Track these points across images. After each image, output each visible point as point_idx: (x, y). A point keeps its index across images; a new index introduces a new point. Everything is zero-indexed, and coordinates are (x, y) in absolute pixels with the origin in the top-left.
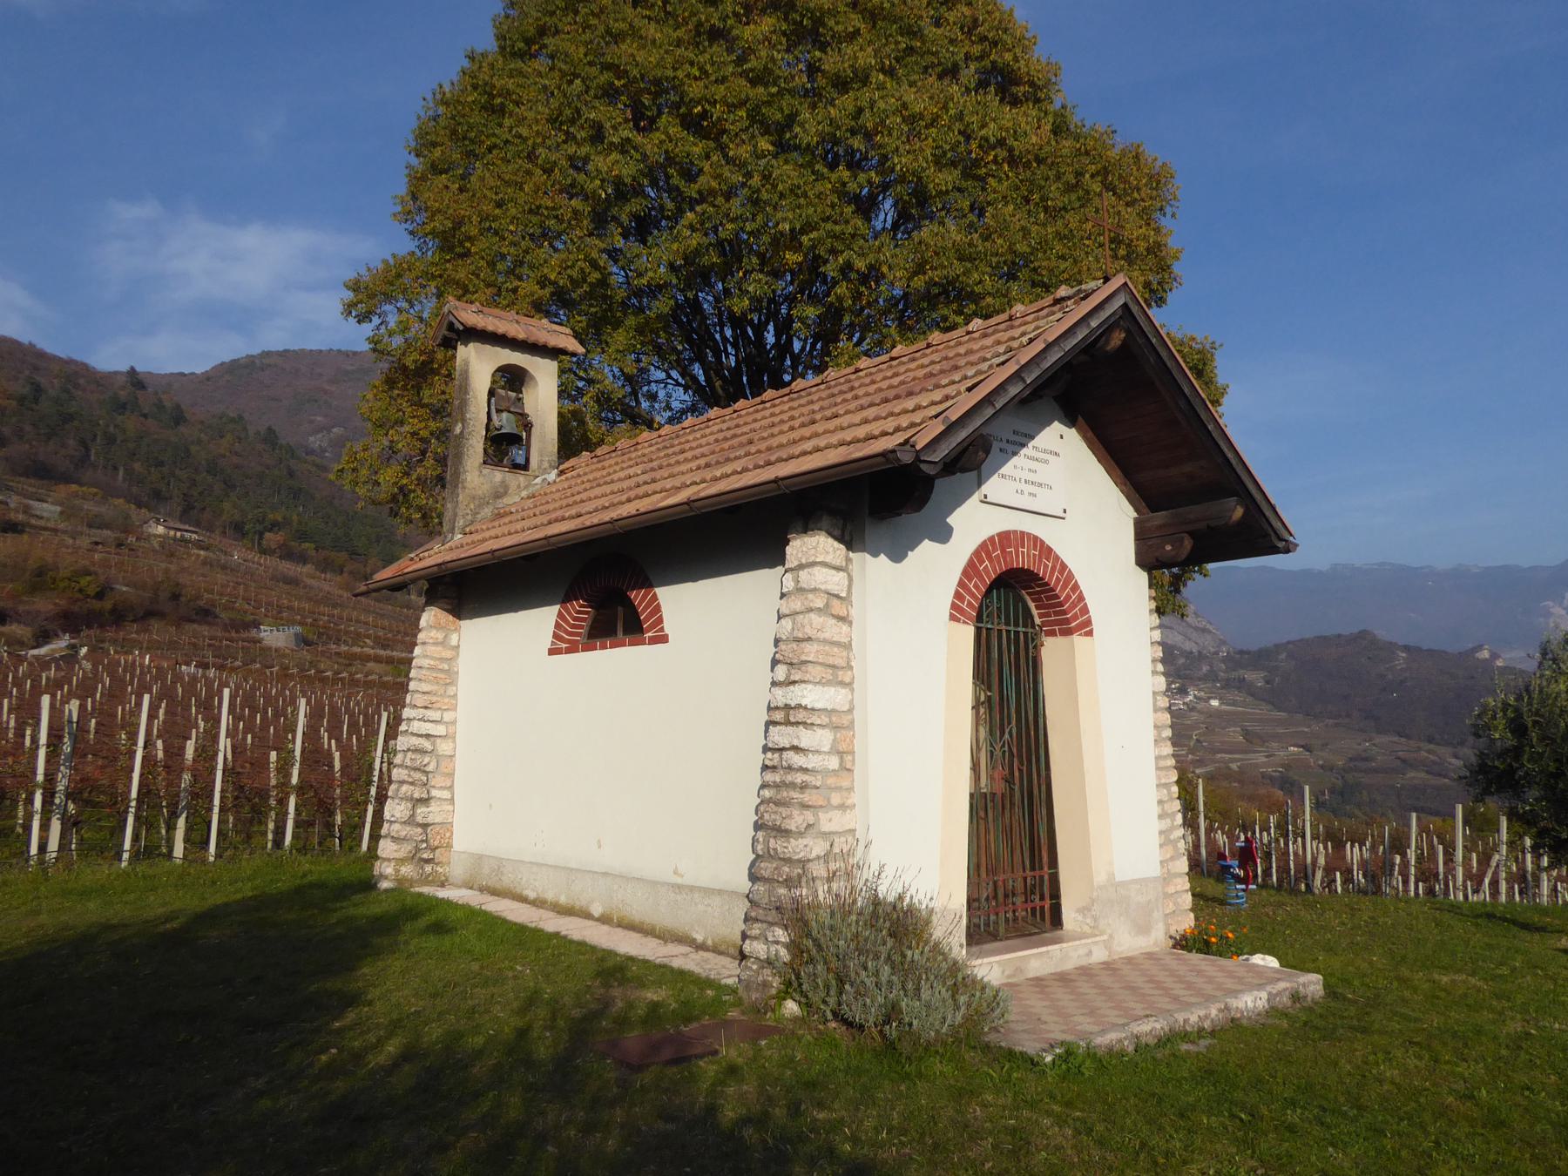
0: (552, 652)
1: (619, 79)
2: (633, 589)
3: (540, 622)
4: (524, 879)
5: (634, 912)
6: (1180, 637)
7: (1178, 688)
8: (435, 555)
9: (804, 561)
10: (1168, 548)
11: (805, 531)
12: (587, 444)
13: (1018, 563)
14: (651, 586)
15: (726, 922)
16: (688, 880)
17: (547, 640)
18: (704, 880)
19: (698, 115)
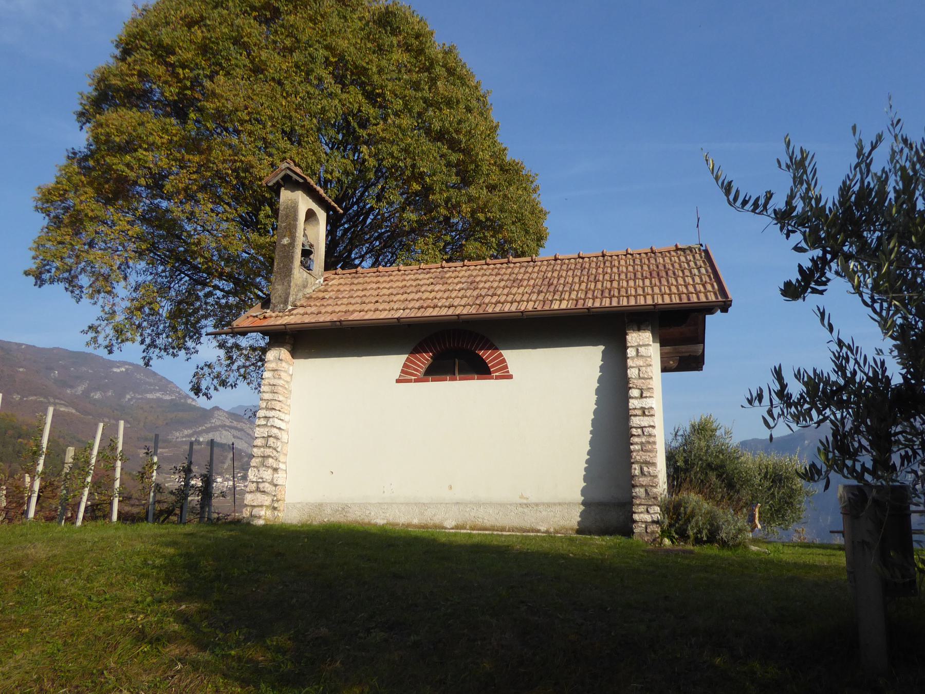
0: (398, 381)
1: (334, 57)
2: (481, 350)
3: (394, 363)
4: (373, 514)
5: (485, 521)
6: (246, 445)
7: (242, 476)
8: (277, 319)
9: (641, 343)
10: (671, 362)
11: (639, 330)
12: (348, 264)
13: (493, 366)
14: (497, 349)
15: (572, 518)
16: (533, 499)
17: (397, 374)
18: (546, 499)
19: (377, 93)
